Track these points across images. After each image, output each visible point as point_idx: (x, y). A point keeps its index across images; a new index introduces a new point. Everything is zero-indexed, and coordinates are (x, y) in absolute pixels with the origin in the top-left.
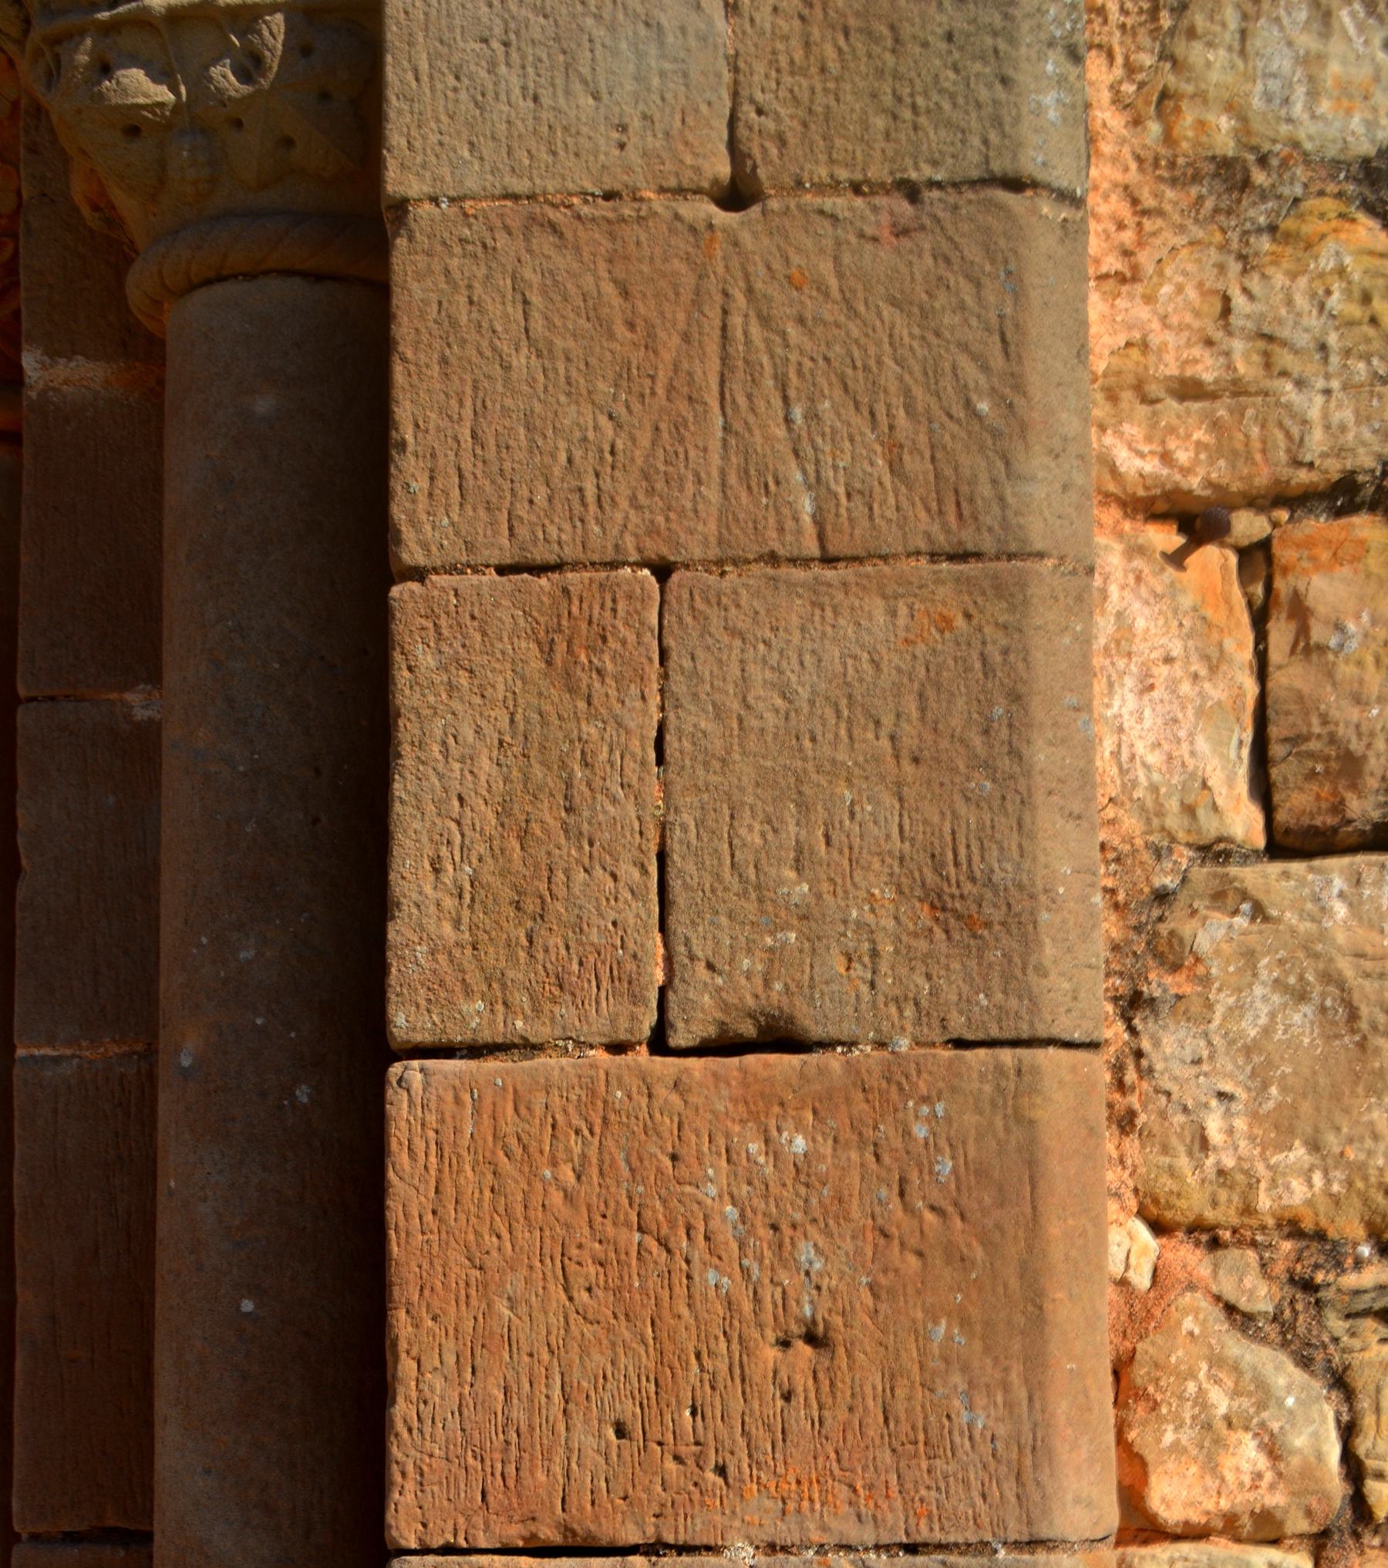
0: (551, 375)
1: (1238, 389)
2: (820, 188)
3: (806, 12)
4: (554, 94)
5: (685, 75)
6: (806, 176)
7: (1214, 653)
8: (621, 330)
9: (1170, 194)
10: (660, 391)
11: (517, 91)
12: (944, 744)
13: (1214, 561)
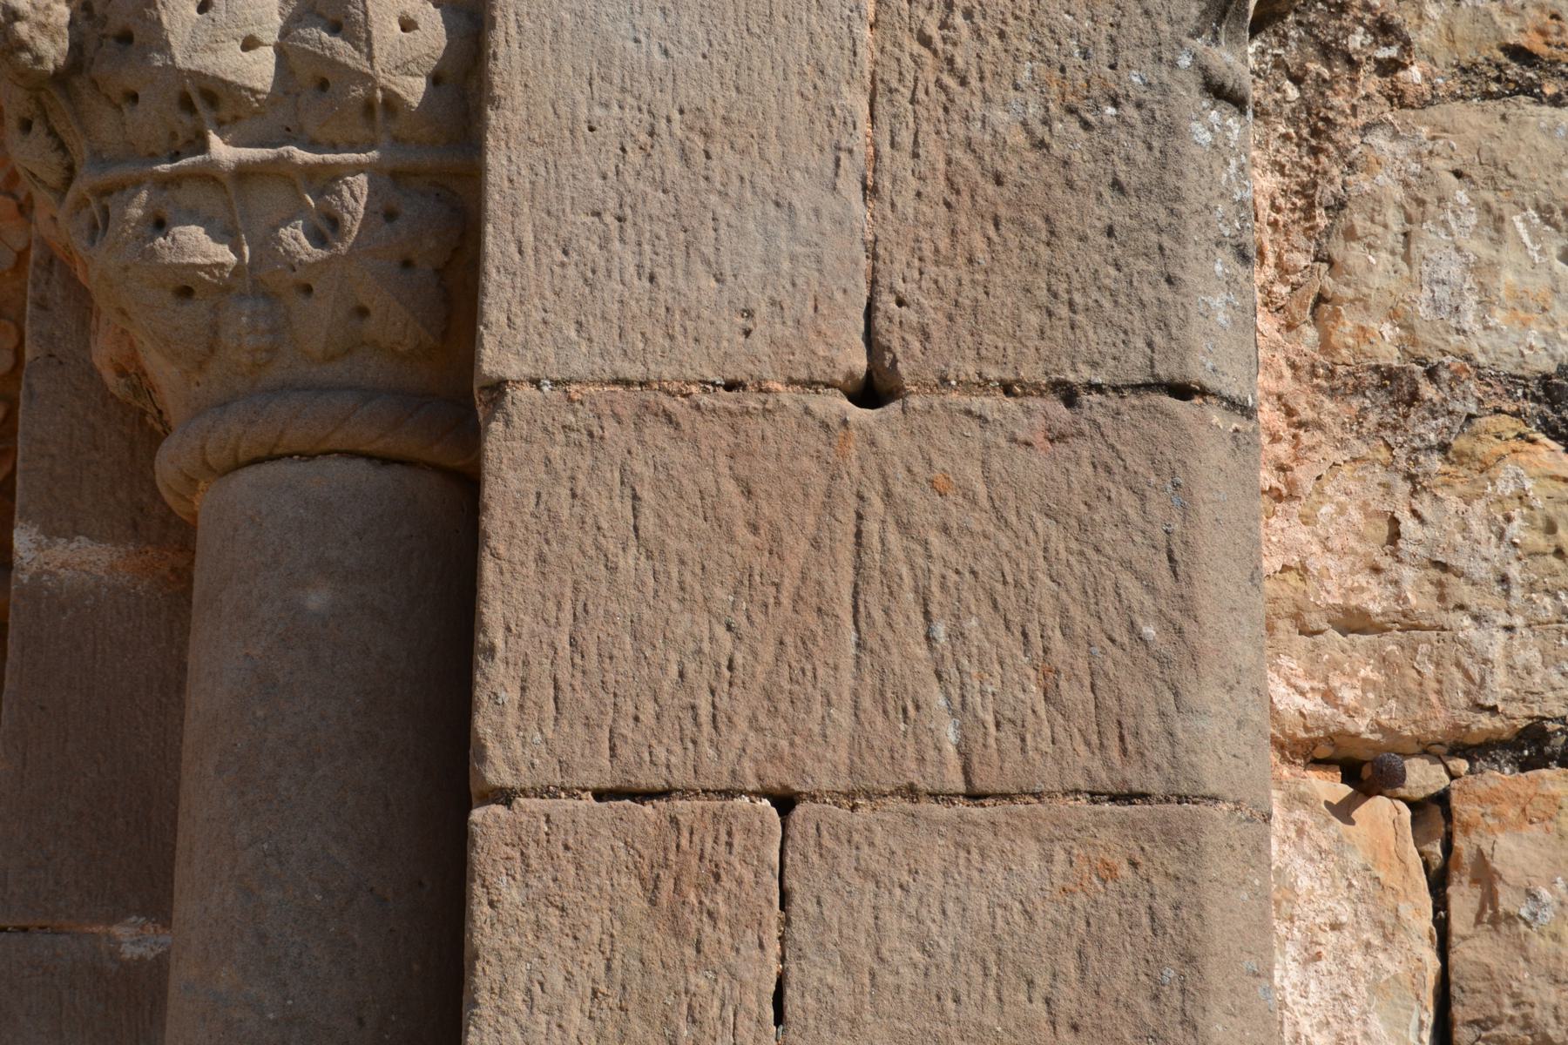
0: (662, 578)
1: (1410, 623)
2: (966, 386)
3: (953, 198)
4: (673, 274)
5: (819, 261)
6: (951, 375)
7: (1389, 921)
8: (742, 532)
9: (1329, 405)
10: (786, 601)
11: (632, 269)
12: (1107, 1010)
13: (1383, 814)
